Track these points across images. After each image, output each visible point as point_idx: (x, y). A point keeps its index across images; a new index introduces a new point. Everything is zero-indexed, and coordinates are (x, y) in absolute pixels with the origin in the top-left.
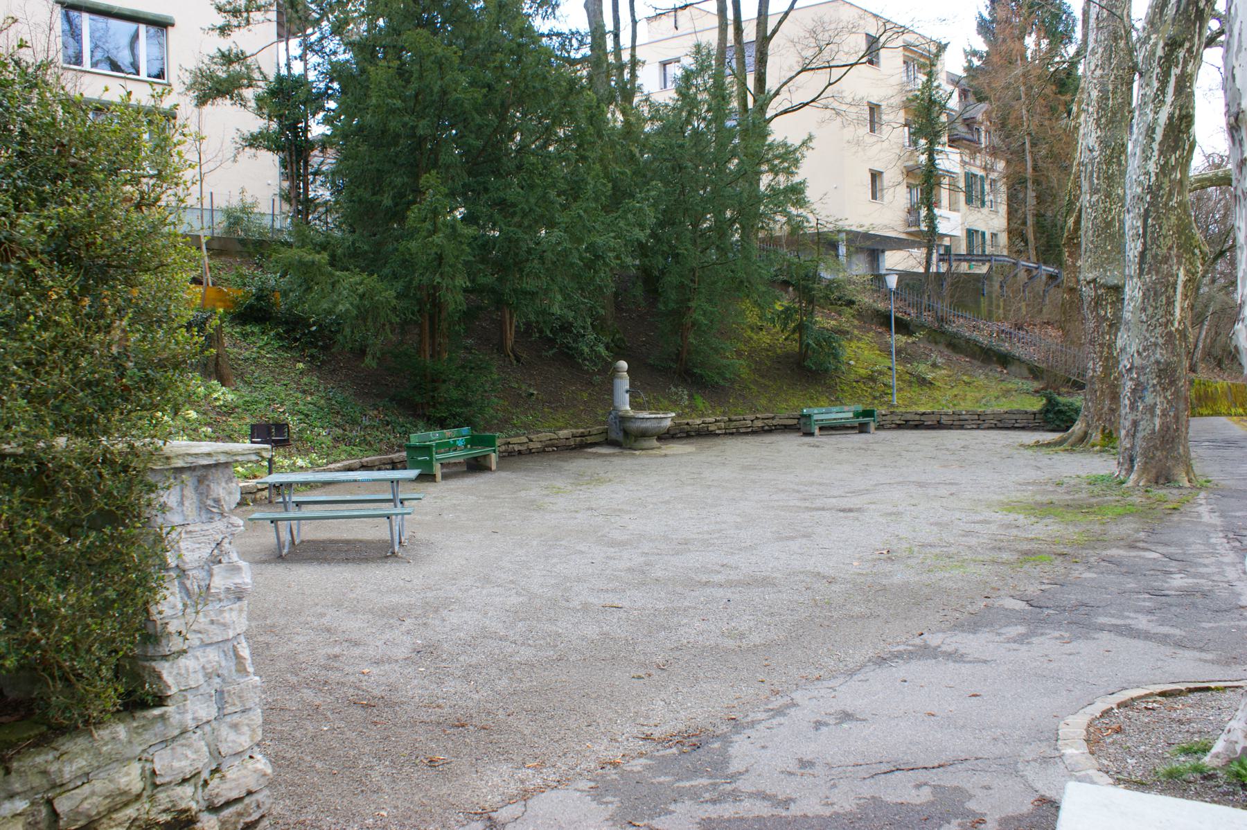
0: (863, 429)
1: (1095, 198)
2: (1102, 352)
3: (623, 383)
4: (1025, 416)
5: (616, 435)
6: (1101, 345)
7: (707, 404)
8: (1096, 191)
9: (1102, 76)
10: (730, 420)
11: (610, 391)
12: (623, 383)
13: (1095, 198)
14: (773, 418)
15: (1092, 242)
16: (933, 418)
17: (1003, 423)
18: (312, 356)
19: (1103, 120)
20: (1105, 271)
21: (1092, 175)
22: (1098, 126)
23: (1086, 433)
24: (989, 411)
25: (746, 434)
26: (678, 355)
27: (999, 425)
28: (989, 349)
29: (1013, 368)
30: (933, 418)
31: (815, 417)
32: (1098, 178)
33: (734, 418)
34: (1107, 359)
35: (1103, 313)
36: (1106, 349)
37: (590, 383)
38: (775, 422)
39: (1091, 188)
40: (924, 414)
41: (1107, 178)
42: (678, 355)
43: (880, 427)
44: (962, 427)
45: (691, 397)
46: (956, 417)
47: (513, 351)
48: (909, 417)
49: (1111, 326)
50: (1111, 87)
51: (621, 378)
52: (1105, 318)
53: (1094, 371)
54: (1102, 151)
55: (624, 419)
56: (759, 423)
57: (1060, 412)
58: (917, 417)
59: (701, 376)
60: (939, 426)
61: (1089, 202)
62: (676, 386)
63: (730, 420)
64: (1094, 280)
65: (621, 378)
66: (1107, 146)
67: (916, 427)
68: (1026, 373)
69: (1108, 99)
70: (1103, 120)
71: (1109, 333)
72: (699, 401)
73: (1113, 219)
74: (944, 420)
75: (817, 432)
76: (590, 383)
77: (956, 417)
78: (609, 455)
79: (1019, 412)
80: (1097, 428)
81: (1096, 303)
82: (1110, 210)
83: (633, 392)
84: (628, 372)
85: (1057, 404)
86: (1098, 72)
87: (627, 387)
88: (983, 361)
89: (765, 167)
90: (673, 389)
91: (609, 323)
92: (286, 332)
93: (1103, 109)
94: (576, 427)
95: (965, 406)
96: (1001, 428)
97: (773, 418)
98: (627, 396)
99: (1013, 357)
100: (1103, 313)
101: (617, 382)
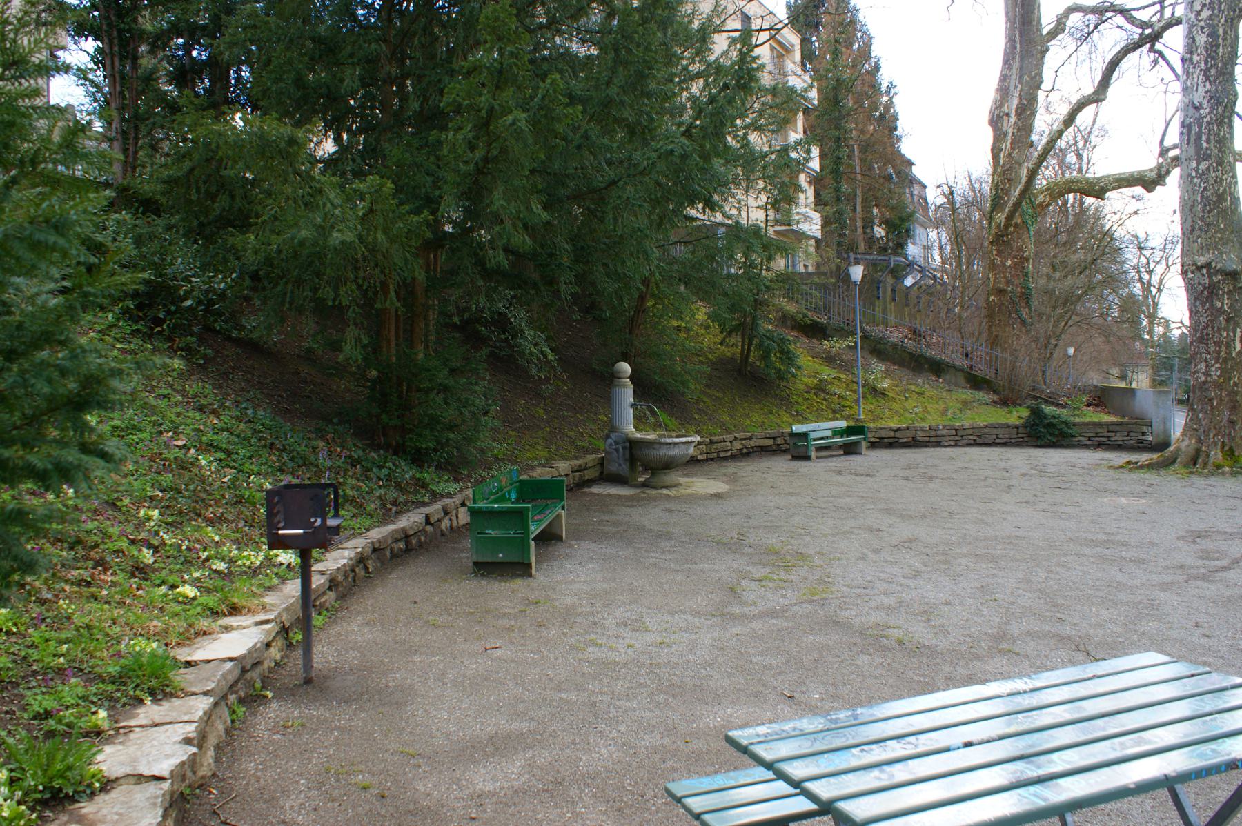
0: (850, 449)
1: (1204, 166)
2: (1218, 353)
3: (626, 395)
4: (1007, 431)
5: (618, 466)
6: (1218, 344)
8: (1206, 157)
9: (1210, 18)
10: (712, 442)
13: (1204, 166)
14: (750, 438)
15: (1202, 219)
16: (910, 434)
17: (983, 439)
18: (187, 349)
19: (1213, 71)
20: (1221, 253)
21: (1199, 138)
22: (1207, 78)
23: (1198, 451)
24: (967, 424)
25: (726, 458)
27: (979, 441)
28: (920, 356)
29: (948, 377)
30: (908, 434)
31: (812, 435)
32: (1208, 142)
33: (715, 438)
34: (1225, 360)
35: (1219, 304)
36: (1223, 349)
37: (539, 396)
38: (753, 443)
39: (1198, 153)
40: (899, 429)
41: (1219, 142)
43: (873, 446)
44: (938, 445)
46: (933, 433)
48: (883, 434)
49: (1228, 320)
50: (1221, 32)
52: (1221, 311)
53: (1207, 374)
54: (1212, 108)
55: (633, 444)
56: (737, 445)
57: (1050, 425)
58: (892, 434)
60: (914, 444)
61: (1197, 170)
63: (712, 442)
64: (1208, 265)
66: (1219, 103)
67: (891, 445)
68: (962, 381)
69: (1217, 46)
70: (1213, 71)
71: (1226, 329)
72: (663, 417)
73: (1225, 190)
74: (920, 436)
75: (813, 454)
76: (539, 396)
77: (933, 433)
78: (628, 498)
79: (1001, 426)
80: (1215, 444)
81: (1211, 293)
82: (1222, 180)
84: (631, 378)
85: (1045, 416)
86: (1205, 14)
88: (913, 370)
92: (139, 307)
93: (1213, 58)
94: (576, 458)
95: (934, 420)
96: (980, 445)
97: (750, 438)
99: (948, 365)
100: (1219, 304)
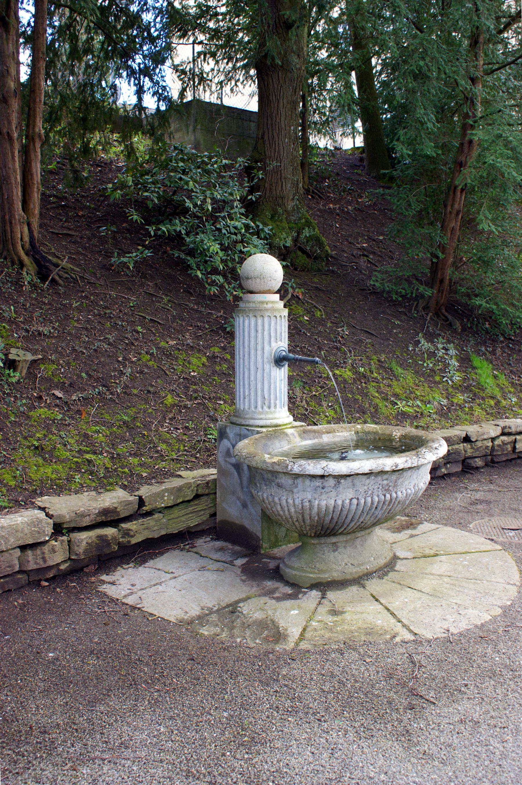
3: (266, 329)
7: (503, 380)
11: (223, 373)
12: (266, 329)
26: (436, 267)
42: (436, 267)
45: (465, 362)
47: (33, 250)
51: (257, 312)
59: (489, 316)
62: (431, 337)
65: (257, 312)
72: (485, 372)
83: (297, 360)
87: (281, 344)
89: (114, 106)
90: (425, 344)
91: (290, 205)
98: (281, 376)
101: (244, 325)
